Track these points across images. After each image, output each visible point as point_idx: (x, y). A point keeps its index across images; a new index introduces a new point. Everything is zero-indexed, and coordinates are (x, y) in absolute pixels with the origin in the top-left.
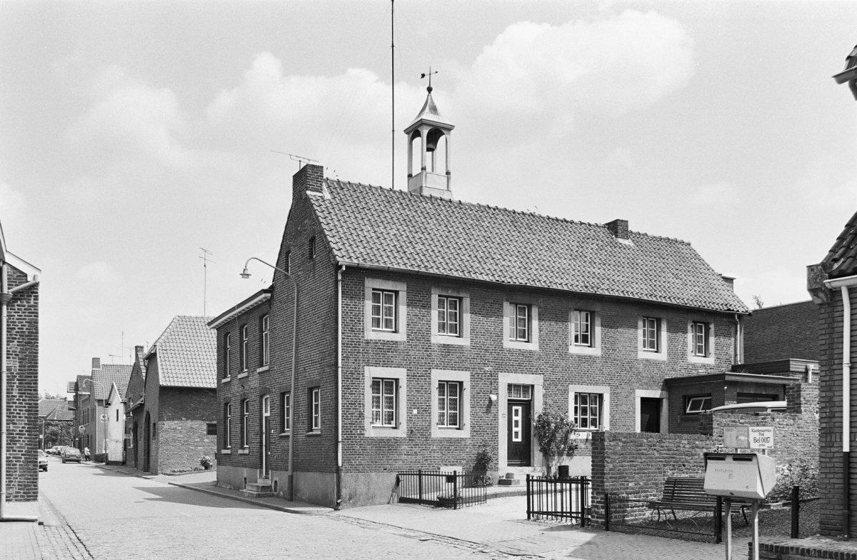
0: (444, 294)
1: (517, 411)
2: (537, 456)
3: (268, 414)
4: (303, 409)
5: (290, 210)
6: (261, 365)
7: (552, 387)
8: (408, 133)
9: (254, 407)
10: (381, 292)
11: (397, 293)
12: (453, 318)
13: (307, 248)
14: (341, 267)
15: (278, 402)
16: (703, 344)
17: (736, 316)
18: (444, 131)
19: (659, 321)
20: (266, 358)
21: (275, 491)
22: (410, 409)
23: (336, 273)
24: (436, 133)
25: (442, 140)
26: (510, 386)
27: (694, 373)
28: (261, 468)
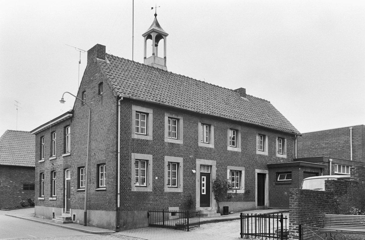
0: (171, 116)
1: (204, 179)
2: (213, 202)
3: (69, 179)
4: (94, 175)
5: (86, 69)
6: (65, 153)
7: (220, 167)
8: (144, 36)
9: (59, 175)
10: (139, 114)
11: (147, 114)
12: (174, 130)
13: (97, 89)
14: (120, 98)
15: (76, 172)
16: (282, 148)
17: (296, 135)
18: (163, 36)
19: (264, 136)
20: (69, 148)
21: (74, 220)
22: (154, 177)
23: (118, 101)
24: (160, 36)
25: (161, 41)
26: (201, 165)
27: (279, 162)
28: (64, 207)
